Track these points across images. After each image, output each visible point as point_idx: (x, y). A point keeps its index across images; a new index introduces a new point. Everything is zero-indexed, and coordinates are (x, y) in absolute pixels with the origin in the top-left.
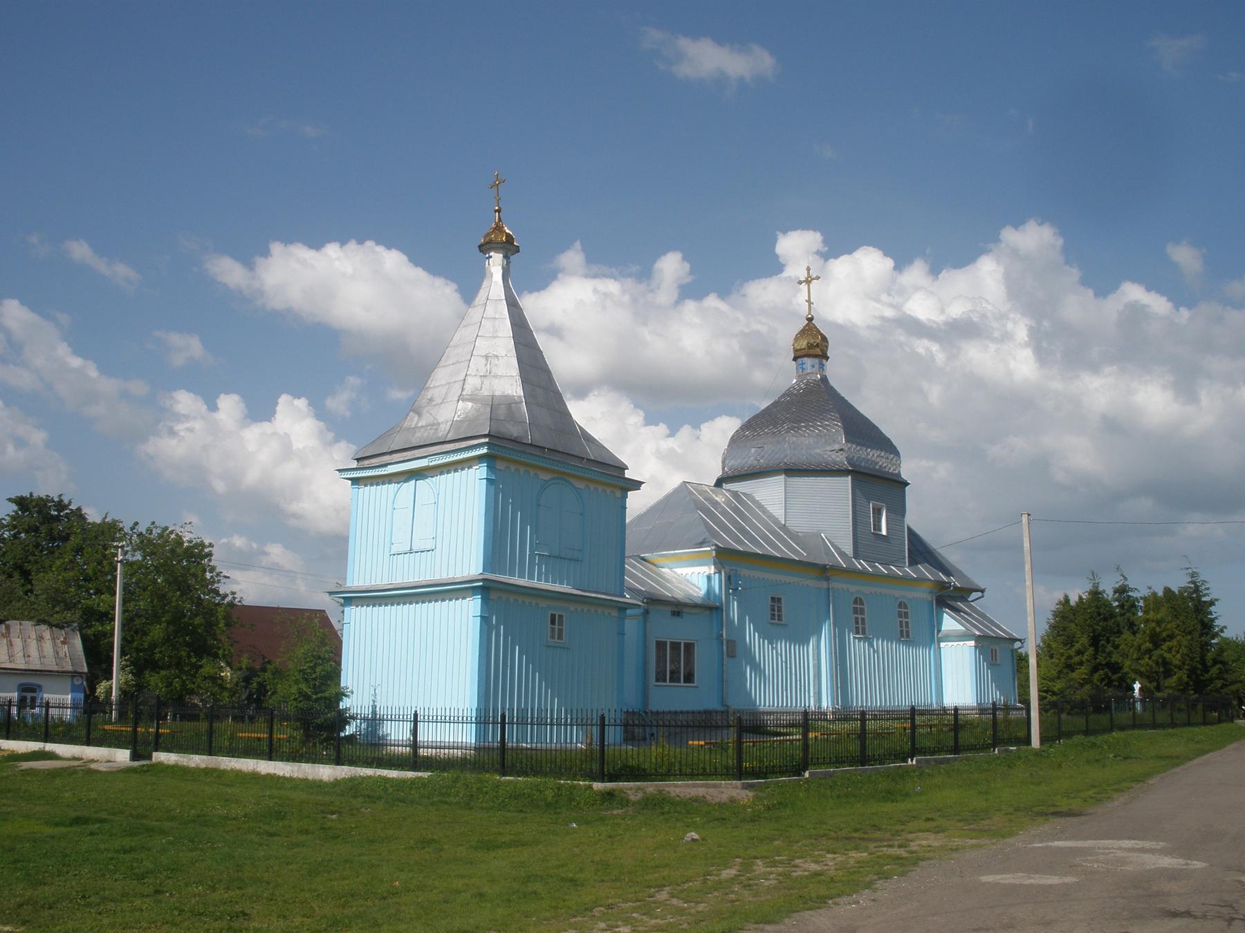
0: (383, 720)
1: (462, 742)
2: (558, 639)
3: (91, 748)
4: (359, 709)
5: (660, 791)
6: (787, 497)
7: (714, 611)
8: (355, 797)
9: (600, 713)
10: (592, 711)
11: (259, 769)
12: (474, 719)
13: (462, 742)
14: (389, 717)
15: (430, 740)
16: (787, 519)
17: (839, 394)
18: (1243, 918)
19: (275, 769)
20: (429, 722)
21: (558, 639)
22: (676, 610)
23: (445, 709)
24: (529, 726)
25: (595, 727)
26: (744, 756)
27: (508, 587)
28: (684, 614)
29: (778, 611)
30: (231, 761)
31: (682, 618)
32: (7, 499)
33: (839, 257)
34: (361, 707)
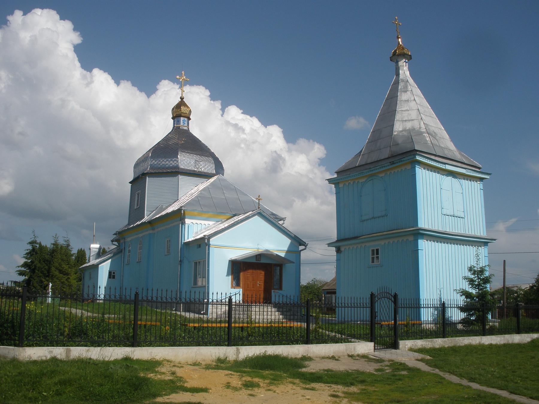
1: (455, 320)
3: (489, 337)
9: (228, 296)
10: (416, 299)
11: (482, 342)
13: (455, 320)
14: (449, 305)
15: (425, 320)
16: (178, 180)
17: (483, 186)
18: (536, 395)
19: (492, 340)
23: (454, 300)
24: (205, 305)
25: (368, 309)
26: (521, 321)
30: (464, 340)
33: (193, 85)
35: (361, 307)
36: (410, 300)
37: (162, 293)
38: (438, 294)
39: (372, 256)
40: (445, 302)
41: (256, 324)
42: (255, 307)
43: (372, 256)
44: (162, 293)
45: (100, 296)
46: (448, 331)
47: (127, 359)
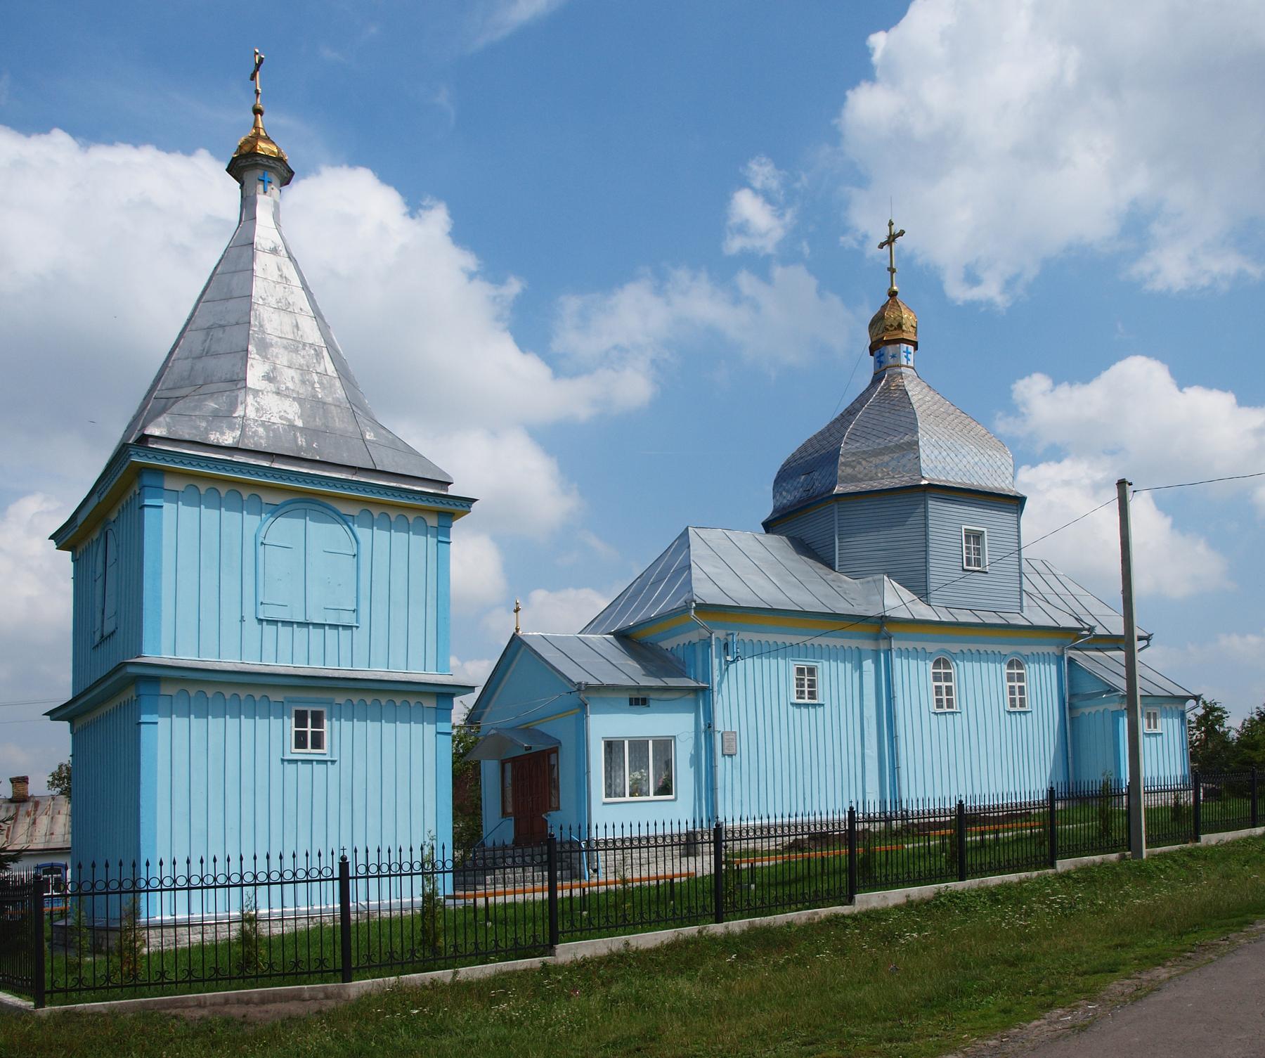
0: (1111, 796)
2: (948, 707)
4: (937, 803)
5: (908, 896)
6: (924, 537)
7: (701, 694)
8: (695, 953)
12: (417, 866)
16: (924, 533)
20: (623, 849)
21: (948, 707)
22: (641, 697)
27: (352, 684)
28: (651, 701)
29: (809, 686)
31: (649, 706)
32: (49, 539)
34: (1158, 778)
35: (860, 822)
36: (1094, 784)
37: (561, 833)
38: (426, 832)
39: (297, 729)
40: (964, 802)
41: (535, 894)
42: (746, 841)
43: (297, 729)
44: (561, 833)
45: (164, 882)
46: (1061, 847)
47: (66, 1011)
